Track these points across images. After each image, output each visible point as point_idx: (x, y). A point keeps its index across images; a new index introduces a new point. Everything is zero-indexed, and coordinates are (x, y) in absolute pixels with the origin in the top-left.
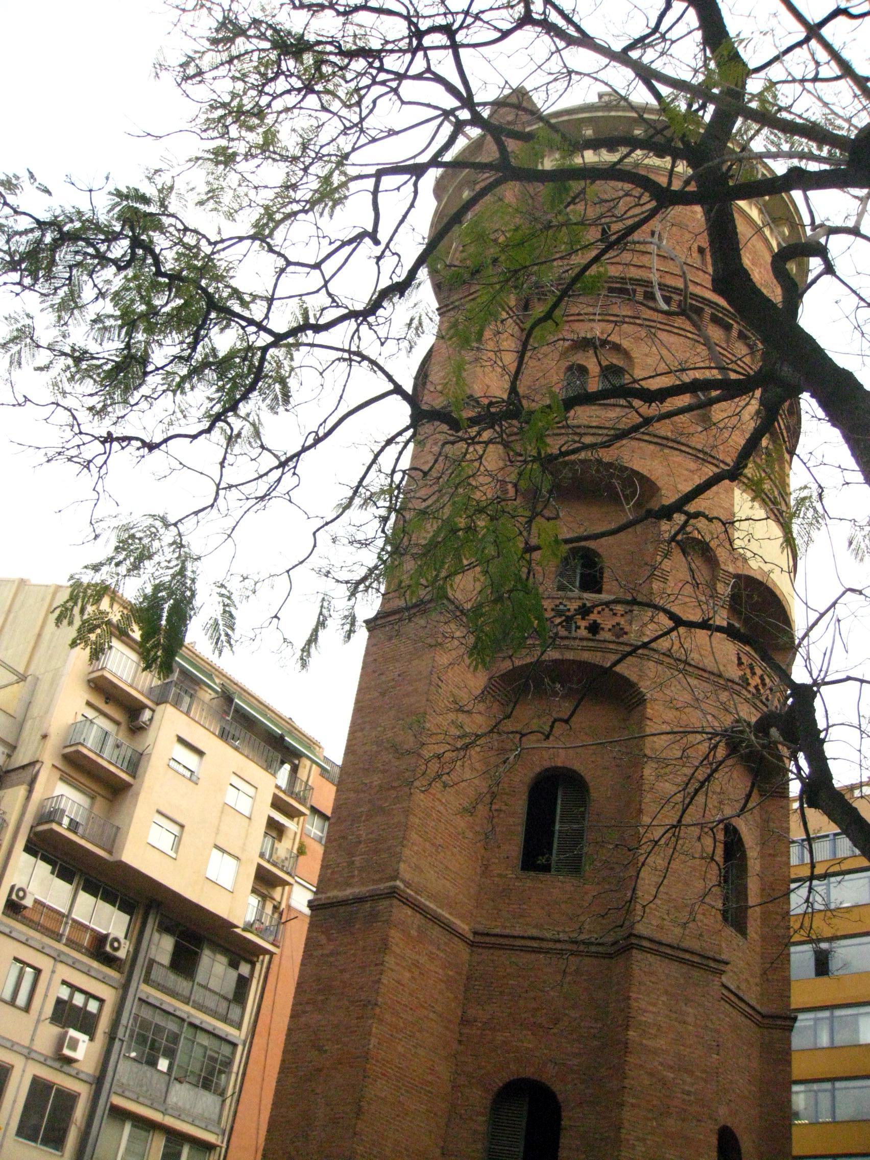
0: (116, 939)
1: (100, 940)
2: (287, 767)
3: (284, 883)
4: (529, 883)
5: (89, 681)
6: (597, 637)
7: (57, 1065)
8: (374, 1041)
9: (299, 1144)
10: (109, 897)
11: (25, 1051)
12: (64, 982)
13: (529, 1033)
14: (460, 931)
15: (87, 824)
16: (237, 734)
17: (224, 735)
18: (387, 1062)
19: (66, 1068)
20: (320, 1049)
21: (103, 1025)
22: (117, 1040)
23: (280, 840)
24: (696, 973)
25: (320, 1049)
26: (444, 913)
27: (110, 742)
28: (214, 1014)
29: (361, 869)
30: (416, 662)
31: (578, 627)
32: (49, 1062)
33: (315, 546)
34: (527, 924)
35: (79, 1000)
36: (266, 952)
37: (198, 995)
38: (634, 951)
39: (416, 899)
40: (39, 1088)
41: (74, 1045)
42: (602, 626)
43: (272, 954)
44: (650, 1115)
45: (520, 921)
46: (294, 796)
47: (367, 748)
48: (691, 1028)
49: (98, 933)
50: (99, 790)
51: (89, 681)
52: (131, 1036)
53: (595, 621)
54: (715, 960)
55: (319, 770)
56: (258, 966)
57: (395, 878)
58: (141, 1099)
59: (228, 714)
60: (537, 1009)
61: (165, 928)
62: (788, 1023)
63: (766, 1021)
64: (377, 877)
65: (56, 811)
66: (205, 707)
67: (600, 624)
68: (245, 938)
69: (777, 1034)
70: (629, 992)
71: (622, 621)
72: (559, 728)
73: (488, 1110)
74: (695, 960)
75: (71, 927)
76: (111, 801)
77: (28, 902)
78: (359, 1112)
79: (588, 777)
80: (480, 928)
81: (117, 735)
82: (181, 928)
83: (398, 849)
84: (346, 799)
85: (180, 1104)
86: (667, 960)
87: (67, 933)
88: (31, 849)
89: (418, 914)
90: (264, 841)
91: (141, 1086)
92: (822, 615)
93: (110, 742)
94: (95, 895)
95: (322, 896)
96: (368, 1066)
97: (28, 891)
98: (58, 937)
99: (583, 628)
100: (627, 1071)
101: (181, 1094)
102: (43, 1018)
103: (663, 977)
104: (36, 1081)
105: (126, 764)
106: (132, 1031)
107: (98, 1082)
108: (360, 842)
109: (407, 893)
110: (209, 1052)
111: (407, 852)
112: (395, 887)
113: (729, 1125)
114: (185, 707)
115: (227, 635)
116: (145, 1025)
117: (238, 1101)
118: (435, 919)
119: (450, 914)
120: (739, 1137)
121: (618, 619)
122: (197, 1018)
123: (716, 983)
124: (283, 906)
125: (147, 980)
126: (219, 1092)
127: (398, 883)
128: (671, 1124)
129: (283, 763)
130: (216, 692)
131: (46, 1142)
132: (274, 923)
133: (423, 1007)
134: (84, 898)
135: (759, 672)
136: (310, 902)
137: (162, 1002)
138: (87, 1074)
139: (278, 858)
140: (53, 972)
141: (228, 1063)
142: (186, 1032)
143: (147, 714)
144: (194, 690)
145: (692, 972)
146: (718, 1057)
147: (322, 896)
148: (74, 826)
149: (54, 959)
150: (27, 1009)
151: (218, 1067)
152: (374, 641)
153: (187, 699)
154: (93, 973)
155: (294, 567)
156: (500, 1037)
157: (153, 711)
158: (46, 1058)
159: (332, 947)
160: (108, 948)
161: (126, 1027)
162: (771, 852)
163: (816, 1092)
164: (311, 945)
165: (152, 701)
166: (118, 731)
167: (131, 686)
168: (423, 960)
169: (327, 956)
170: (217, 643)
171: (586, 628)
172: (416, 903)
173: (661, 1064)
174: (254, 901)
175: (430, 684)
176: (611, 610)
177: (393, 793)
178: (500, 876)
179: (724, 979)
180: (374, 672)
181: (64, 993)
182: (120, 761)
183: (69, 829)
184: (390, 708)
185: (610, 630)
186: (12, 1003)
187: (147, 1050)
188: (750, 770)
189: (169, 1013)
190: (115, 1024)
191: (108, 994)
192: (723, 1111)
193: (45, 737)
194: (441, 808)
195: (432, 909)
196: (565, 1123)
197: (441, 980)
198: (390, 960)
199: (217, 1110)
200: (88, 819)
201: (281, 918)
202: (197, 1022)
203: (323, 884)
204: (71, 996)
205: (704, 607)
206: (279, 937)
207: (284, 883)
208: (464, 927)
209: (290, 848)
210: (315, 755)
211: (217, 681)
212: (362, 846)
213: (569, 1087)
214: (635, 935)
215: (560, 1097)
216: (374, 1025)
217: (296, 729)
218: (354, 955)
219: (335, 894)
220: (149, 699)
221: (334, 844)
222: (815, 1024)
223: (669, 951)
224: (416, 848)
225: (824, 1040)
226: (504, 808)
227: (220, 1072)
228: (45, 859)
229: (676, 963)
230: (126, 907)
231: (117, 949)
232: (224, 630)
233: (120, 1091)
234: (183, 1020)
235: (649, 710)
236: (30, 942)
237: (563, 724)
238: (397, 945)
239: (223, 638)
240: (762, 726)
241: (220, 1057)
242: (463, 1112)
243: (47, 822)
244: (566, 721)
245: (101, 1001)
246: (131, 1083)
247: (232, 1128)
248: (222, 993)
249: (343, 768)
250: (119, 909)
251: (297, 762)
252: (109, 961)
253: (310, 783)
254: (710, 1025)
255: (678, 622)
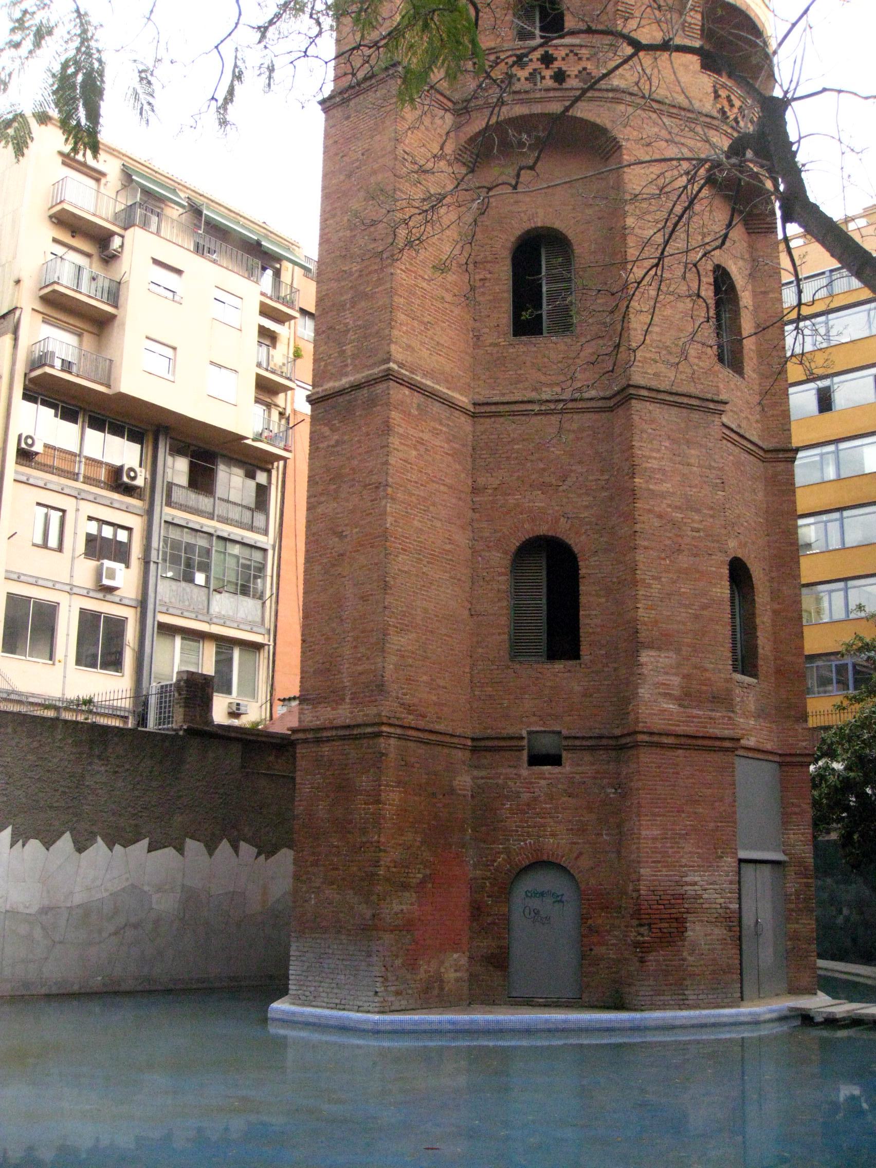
0: (131, 469)
1: (116, 472)
2: (269, 273)
3: (286, 389)
4: (522, 349)
5: (51, 217)
6: (565, 85)
7: (100, 595)
8: (390, 520)
9: (334, 625)
10: (117, 430)
11: (67, 588)
12: (90, 518)
13: (539, 492)
14: (460, 404)
15: (79, 363)
16: (212, 247)
17: (199, 250)
18: (407, 538)
19: (109, 597)
20: (341, 535)
21: (136, 551)
22: (152, 563)
23: (274, 347)
24: (696, 416)
25: (341, 535)
26: (441, 389)
27: (86, 276)
28: (240, 525)
29: (354, 357)
30: (378, 137)
31: (543, 78)
32: (92, 594)
33: (240, 14)
34: (526, 389)
35: (107, 532)
36: (279, 458)
37: (221, 509)
38: (633, 401)
39: (412, 379)
40: (88, 620)
41: (112, 574)
42: (568, 73)
43: (285, 459)
44: (663, 555)
45: (518, 386)
46: (281, 301)
47: (341, 234)
48: (695, 469)
49: (112, 466)
50: (85, 327)
51: (51, 217)
52: (164, 560)
53: (560, 69)
54: (713, 401)
55: (302, 271)
56: (274, 472)
57: (388, 360)
58: (186, 614)
59: (200, 228)
60: (544, 470)
61: (177, 450)
62: (790, 455)
63: (769, 456)
64: (371, 361)
65: (46, 354)
66: (175, 224)
67: (552, 55)
68: (257, 448)
69: (781, 466)
70: (631, 441)
71: (589, 66)
72: (526, 175)
73: (508, 570)
74: (695, 403)
75: (86, 464)
76: (98, 335)
77: (38, 448)
78: (386, 587)
79: (570, 234)
80: (481, 399)
81: (90, 267)
82: (192, 448)
83: (387, 332)
84: (328, 290)
85: (223, 613)
86: (666, 407)
87: (82, 471)
88: (29, 396)
89: (416, 393)
90: (258, 353)
91: (184, 602)
92: (794, 25)
93: (86, 276)
94: (102, 430)
95: (320, 389)
96: (388, 544)
97: (35, 437)
98: (74, 476)
99: (548, 77)
100: (637, 517)
101: (223, 604)
102: (77, 554)
103: (664, 423)
104: (83, 612)
105: (105, 295)
106: (165, 553)
107: (142, 605)
108: (349, 330)
109: (402, 374)
110: (241, 561)
111: (395, 332)
112: (389, 369)
113: (739, 556)
114: (154, 228)
115: (149, 104)
116: (176, 545)
117: (277, 602)
118: (432, 395)
119: (448, 389)
120: (749, 565)
121: (584, 64)
122: (222, 530)
123: (716, 423)
124: (288, 412)
125: (169, 503)
126: (258, 595)
127: (392, 365)
128: (684, 561)
129: (264, 269)
130: (183, 206)
131: (105, 665)
132: (282, 429)
133: (433, 481)
134: (93, 435)
135: (737, 103)
136: (308, 397)
137: (188, 521)
138: (131, 599)
139: (275, 365)
140: (77, 510)
141: (261, 568)
142: (216, 546)
143: (116, 242)
144: (160, 208)
145: (692, 415)
146: (723, 493)
147: (320, 389)
148: (67, 366)
149: (76, 497)
150: (60, 549)
151: (252, 573)
152: (331, 122)
153: (154, 219)
154: (116, 505)
155: (222, 42)
156: (511, 501)
157: (123, 237)
158: (89, 590)
159: (336, 437)
160: (125, 479)
161: (158, 550)
162: (763, 289)
163: (826, 522)
164: (315, 440)
165: (118, 226)
166: (91, 263)
167: (94, 215)
168: (426, 436)
169: (333, 446)
170: (141, 114)
171: (551, 77)
172: (413, 382)
173: (669, 506)
174: (260, 409)
175: (396, 159)
176: (576, 54)
177: (375, 277)
178: (491, 345)
179: (725, 419)
180: (337, 154)
181: (93, 528)
182: (99, 294)
183: (62, 370)
184: (359, 190)
185: (576, 76)
186: (45, 545)
187: (182, 567)
188: (727, 198)
189: (197, 531)
190: (147, 548)
191: (136, 523)
192: (732, 544)
193: (18, 282)
194: (424, 285)
195: (428, 386)
196: (582, 572)
197: (447, 454)
198: (395, 441)
199: (259, 613)
200: (80, 359)
201: (288, 423)
202: (225, 535)
203: (319, 376)
204: (100, 530)
205: (664, 26)
206: (290, 443)
207: (286, 389)
208: (463, 399)
209: (286, 353)
210: (296, 257)
211: (182, 195)
212: (351, 333)
213: (583, 538)
214: (632, 386)
215: (576, 550)
216: (388, 505)
217: (271, 232)
218: (359, 442)
219: (331, 385)
220: (114, 224)
221: (323, 336)
222: (822, 458)
223: (668, 398)
224: (405, 328)
225: (831, 473)
226: (488, 276)
227: (256, 577)
228: (45, 403)
229: (676, 408)
230: (136, 436)
231: (134, 478)
232: (145, 99)
233: (164, 610)
234: (211, 535)
235: (625, 157)
236: (49, 486)
237: (529, 172)
238: (399, 425)
239: (146, 107)
240: (737, 149)
241: (253, 564)
242: (485, 574)
243: (39, 367)
244: (532, 168)
245: (129, 530)
246: (173, 600)
247: (276, 626)
248: (244, 504)
249: (320, 262)
250: (128, 440)
251: (278, 266)
252: (129, 490)
253: (295, 285)
254: (713, 464)
255: (638, 46)
